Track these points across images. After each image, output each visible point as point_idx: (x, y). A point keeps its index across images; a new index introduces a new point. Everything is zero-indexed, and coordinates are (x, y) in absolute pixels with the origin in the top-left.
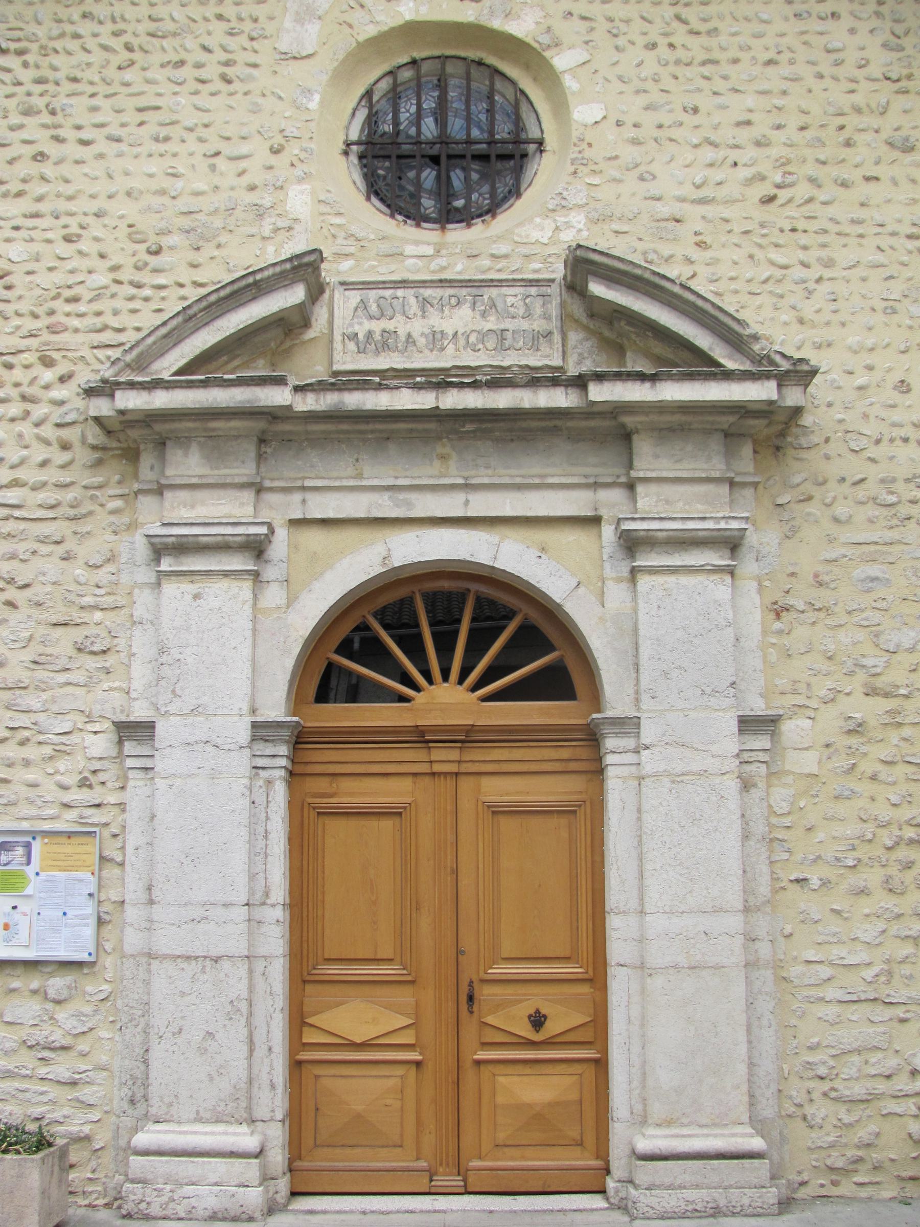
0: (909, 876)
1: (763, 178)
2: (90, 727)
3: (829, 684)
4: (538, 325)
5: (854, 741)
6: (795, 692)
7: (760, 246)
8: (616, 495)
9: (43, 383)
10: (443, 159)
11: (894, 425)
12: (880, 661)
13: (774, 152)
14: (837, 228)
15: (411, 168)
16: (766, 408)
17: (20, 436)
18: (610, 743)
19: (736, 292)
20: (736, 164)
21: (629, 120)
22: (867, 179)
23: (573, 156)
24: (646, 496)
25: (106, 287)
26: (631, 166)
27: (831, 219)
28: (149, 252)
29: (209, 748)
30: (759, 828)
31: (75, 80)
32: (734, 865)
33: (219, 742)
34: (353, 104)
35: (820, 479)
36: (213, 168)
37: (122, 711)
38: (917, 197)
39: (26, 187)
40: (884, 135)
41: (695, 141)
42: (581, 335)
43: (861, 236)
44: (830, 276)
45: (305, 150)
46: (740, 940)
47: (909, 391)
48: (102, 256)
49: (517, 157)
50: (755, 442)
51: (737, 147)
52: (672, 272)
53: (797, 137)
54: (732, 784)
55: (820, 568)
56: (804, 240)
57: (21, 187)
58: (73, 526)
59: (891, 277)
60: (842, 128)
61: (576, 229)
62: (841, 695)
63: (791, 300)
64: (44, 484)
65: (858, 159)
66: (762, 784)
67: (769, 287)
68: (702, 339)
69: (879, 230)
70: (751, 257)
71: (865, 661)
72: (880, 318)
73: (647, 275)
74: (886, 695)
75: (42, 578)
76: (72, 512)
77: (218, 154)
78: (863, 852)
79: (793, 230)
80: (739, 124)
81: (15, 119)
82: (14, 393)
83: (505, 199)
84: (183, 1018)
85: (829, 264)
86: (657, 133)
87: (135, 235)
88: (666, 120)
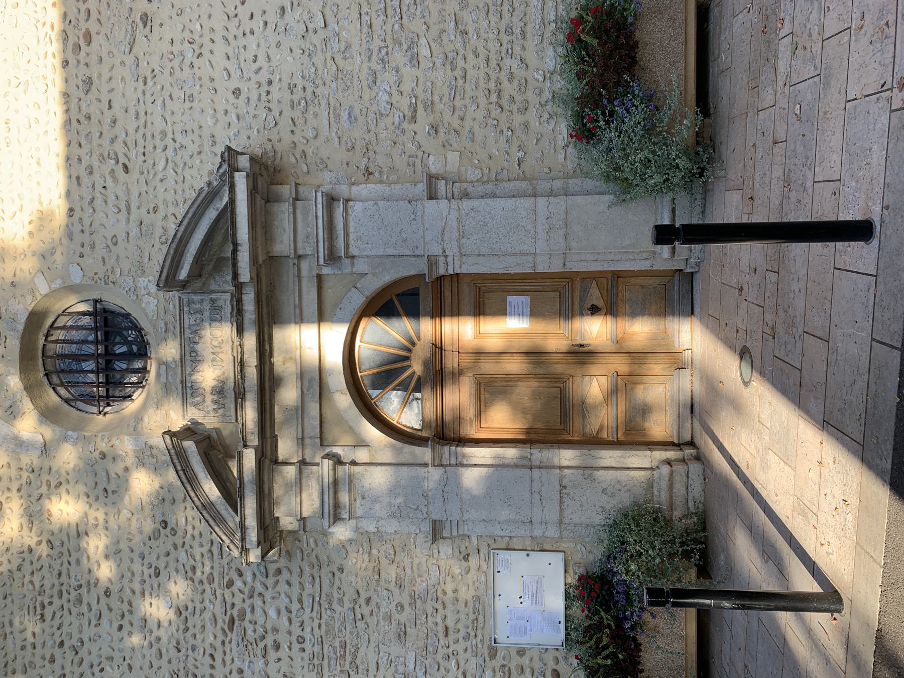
0: (518, 98)
2: (436, 556)
3: (410, 145)
4: (207, 306)
5: (442, 130)
6: (414, 165)
7: (155, 175)
8: (305, 265)
10: (109, 358)
11: (259, 99)
12: (397, 113)
13: (96, 163)
15: (114, 377)
16: (251, 178)
18: (442, 271)
19: (183, 190)
21: (79, 250)
22: (110, 107)
25: (187, 552)
28: (165, 528)
30: (490, 187)
31: (60, 574)
32: (510, 203)
34: (74, 410)
35: (293, 145)
36: (114, 492)
39: (126, 600)
40: (82, 95)
41: (91, 211)
43: (146, 113)
46: (552, 199)
47: (239, 90)
48: (168, 554)
49: (106, 315)
50: (272, 184)
51: (93, 186)
52: (172, 227)
54: (466, 204)
55: (344, 148)
56: (150, 148)
59: (170, 96)
60: (79, 121)
61: (148, 283)
64: (300, 583)
65: (98, 112)
66: (465, 185)
67: (179, 171)
68: (211, 215)
69: (141, 101)
70: (162, 180)
71: (397, 123)
72: (195, 104)
74: (416, 111)
75: (353, 584)
76: (316, 567)
77: (105, 490)
78: (504, 126)
79: (144, 154)
80: (79, 184)
81: (84, 608)
82: (248, 602)
83: (131, 322)
85: (164, 134)
86: (87, 233)
87: (155, 535)
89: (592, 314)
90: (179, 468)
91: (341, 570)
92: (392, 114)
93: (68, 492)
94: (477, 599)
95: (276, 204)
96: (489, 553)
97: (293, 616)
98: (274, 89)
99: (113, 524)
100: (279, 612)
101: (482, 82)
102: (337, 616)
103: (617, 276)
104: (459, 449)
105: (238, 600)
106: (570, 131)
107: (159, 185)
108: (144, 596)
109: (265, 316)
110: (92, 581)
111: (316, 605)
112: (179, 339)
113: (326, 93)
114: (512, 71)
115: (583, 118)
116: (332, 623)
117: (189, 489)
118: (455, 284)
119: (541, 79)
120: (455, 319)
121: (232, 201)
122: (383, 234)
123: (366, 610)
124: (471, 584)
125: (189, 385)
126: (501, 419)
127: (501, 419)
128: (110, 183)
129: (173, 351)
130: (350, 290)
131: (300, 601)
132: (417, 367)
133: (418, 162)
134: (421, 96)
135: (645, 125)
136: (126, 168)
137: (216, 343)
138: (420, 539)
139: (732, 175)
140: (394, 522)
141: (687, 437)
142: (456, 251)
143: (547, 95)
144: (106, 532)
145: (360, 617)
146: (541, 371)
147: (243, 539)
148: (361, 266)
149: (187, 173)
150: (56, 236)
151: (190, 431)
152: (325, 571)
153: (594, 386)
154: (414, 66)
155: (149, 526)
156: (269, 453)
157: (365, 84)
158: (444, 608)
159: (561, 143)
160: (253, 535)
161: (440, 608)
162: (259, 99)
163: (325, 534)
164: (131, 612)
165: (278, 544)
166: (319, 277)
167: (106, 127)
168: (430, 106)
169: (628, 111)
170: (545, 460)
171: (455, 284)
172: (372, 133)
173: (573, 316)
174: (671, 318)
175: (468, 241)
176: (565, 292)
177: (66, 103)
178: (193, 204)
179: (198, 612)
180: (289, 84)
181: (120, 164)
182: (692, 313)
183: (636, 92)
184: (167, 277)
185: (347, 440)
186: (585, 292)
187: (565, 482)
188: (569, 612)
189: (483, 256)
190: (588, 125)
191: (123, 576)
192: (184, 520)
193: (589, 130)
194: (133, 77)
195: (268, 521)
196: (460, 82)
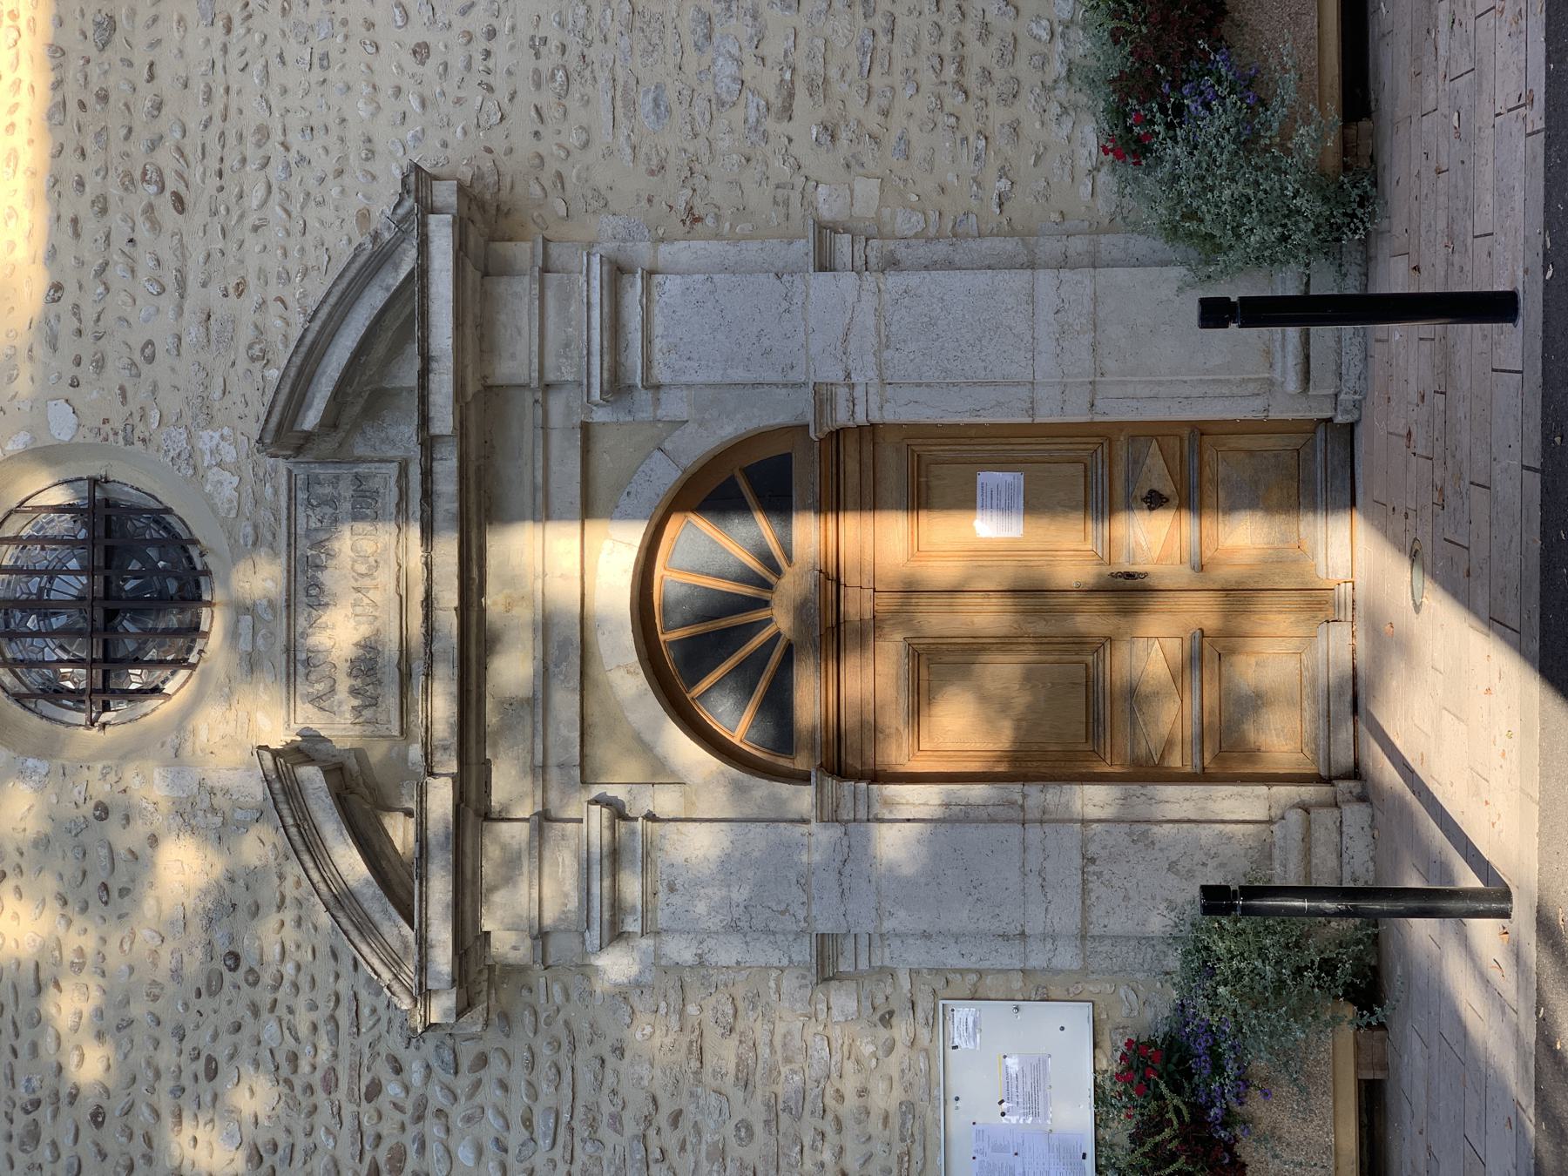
0: (999, 73)
1: (150, 208)
2: (822, 1017)
3: (778, 163)
4: (346, 490)
5: (844, 136)
6: (787, 203)
7: (242, 217)
8: (557, 405)
9: (403, 1095)
10: (111, 605)
11: (468, 67)
13: (114, 192)
14: (217, 119)
17: (468, 1119)
18: (842, 418)
19: (302, 250)
20: (131, 241)
22: (151, 78)
23: (121, 442)
24: (559, 369)
25: (280, 1021)
26: (134, 371)
27: (206, 127)
28: (234, 969)
29: (847, 870)
30: (941, 249)
32: (982, 279)
33: (839, 858)
34: (35, 720)
35: (537, 161)
36: (124, 892)
37: (804, 977)
38: (175, 18)
40: (93, 52)
41: (101, 289)
42: (358, 439)
43: (227, 90)
44: (280, 132)
45: (104, 776)
46: (1066, 274)
47: (426, 46)
48: (238, 1028)
50: (492, 239)
51: (108, 237)
53: (94, 161)
54: (893, 282)
56: (232, 160)
57: (139, 1139)
58: (582, 1046)
59: (281, 56)
62: (791, 149)
63: (311, 183)
64: (530, 1084)
66: (891, 245)
68: (375, 298)
69: (219, 66)
70: (256, 229)
71: (752, 120)
72: (332, 74)
73: (297, 360)
74: (791, 95)
75: (645, 1083)
76: (565, 1046)
77: (105, 887)
78: (969, 128)
79: (220, 174)
80: (77, 234)
81: (45, 1153)
82: (412, 1130)
83: (167, 528)
84: (1153, 898)
85: (263, 133)
86: (88, 338)
87: (213, 985)
88: (71, 323)
89: (1151, 509)
90: (290, 821)
91: (619, 1051)
92: (742, 101)
93: (18, 891)
94: (908, 1108)
95: (505, 279)
96: (935, 1010)
97: (511, 1159)
98: (500, 46)
99: (116, 961)
100: (479, 1151)
101: (926, 42)
102: (607, 1154)
103: (1200, 430)
104: (874, 787)
105: (388, 1128)
106: (1103, 142)
107: (250, 238)
108: (180, 1123)
109: (473, 508)
110: (64, 1091)
111: (562, 1130)
112: (284, 559)
113: (609, 57)
114: (988, 19)
115: (1126, 115)
116: (596, 1170)
117: (310, 865)
118: (867, 448)
119: (1045, 36)
120: (868, 517)
121: (422, 272)
122: (728, 340)
123: (671, 1140)
124: (896, 1076)
125: (302, 656)
126: (959, 728)
127: (959, 728)
128: (143, 232)
129: (269, 584)
130: (649, 456)
131: (528, 1123)
132: (782, 620)
133: (795, 198)
134: (804, 67)
135: (1239, 134)
136: (179, 203)
137: (363, 569)
138: (789, 983)
139: (1398, 229)
140: (736, 940)
141: (1344, 758)
142: (872, 374)
143: (1057, 68)
144: (101, 981)
145: (658, 1155)
146: (1041, 627)
147: (422, 968)
148: (674, 406)
149: (312, 214)
150: (22, 342)
151: (306, 750)
152: (584, 1055)
153: (1151, 651)
154: (790, 7)
155: (194, 964)
156: (473, 796)
157: (688, 40)
158: (839, 1130)
159: (1084, 164)
160: (442, 959)
161: (829, 1129)
162: (468, 67)
163: (585, 970)
164: (149, 1160)
165: (483, 996)
166: (586, 428)
167: (140, 117)
168: (820, 87)
169: (1207, 106)
170: (1052, 807)
171: (867, 448)
172: (701, 140)
173: (1111, 513)
174: (1310, 517)
175: (897, 355)
176: (1092, 467)
177: (57, 67)
178: (341, 276)
179: (299, 1156)
180: (532, 38)
181: (167, 194)
182: (1353, 504)
183: (1223, 71)
184: (280, 425)
185: (631, 768)
186: (1135, 462)
187: (1093, 849)
188: (1107, 1135)
189: (928, 385)
190: (1136, 130)
191: (134, 1080)
192: (277, 949)
193: (1139, 140)
194: (204, 16)
195: (469, 939)
196: (883, 40)
